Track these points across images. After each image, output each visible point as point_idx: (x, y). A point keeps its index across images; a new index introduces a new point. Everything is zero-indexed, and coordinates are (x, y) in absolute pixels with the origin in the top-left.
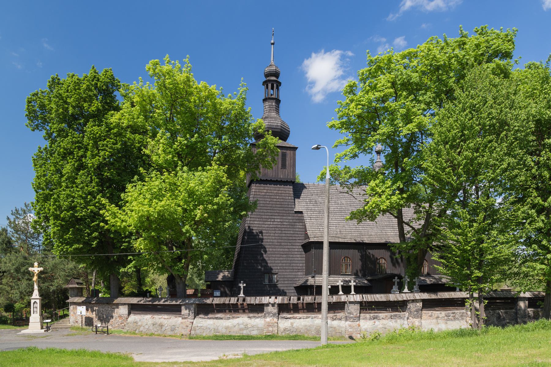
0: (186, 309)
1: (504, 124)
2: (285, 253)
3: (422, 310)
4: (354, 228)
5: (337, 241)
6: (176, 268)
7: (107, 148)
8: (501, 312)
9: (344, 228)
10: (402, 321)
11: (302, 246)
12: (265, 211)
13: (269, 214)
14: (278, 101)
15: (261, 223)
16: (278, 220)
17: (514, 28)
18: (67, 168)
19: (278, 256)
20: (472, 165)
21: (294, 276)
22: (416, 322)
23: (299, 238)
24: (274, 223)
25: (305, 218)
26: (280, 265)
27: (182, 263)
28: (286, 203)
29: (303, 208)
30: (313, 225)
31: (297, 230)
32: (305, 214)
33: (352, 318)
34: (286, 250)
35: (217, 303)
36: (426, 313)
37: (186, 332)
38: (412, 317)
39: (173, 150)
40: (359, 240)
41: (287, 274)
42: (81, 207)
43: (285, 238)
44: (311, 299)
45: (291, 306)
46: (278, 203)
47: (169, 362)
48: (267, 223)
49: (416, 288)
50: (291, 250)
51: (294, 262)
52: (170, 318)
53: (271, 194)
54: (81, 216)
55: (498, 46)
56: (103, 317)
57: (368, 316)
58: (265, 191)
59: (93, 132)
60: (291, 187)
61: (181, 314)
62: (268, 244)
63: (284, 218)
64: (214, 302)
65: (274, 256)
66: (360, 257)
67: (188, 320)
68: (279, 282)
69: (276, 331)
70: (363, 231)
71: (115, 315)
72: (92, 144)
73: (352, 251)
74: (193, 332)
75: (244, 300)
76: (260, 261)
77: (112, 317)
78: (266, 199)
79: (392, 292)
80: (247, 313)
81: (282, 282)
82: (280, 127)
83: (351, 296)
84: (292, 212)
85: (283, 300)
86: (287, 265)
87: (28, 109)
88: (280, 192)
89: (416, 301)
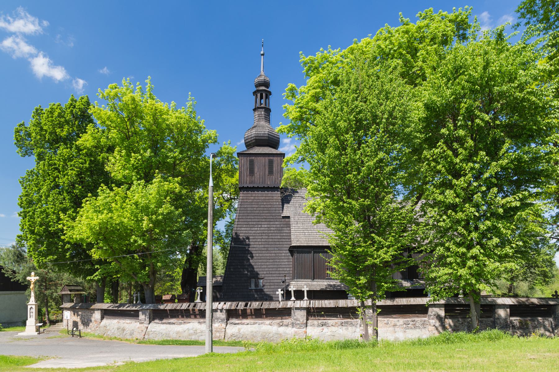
0: (143, 314)
2: (272, 258)
5: (321, 245)
6: (140, 275)
7: (74, 168)
10: (354, 328)
12: (253, 217)
13: (257, 220)
14: (268, 111)
15: (248, 229)
16: (265, 226)
19: (265, 261)
23: (286, 243)
24: (261, 229)
26: (267, 269)
27: (145, 271)
28: (274, 209)
29: (291, 213)
30: (299, 229)
31: (284, 234)
32: (292, 219)
33: (298, 324)
34: (273, 255)
35: (170, 308)
36: (313, 321)
37: (140, 337)
39: (131, 166)
43: (272, 243)
44: (258, 305)
45: (240, 312)
46: (265, 209)
48: (254, 229)
50: (277, 254)
51: (281, 266)
53: (258, 201)
54: (54, 230)
56: (85, 321)
57: (316, 322)
58: (252, 198)
59: (62, 154)
62: (254, 249)
63: (272, 223)
65: (261, 261)
68: (266, 287)
69: (223, 337)
71: (93, 319)
74: (146, 337)
76: (247, 267)
77: (91, 321)
78: (253, 206)
79: (349, 298)
80: (198, 318)
81: (268, 287)
82: (267, 135)
83: (291, 302)
84: (279, 217)
85: (231, 305)
86: (274, 269)
87: (16, 137)
88: (267, 198)
89: (369, 308)
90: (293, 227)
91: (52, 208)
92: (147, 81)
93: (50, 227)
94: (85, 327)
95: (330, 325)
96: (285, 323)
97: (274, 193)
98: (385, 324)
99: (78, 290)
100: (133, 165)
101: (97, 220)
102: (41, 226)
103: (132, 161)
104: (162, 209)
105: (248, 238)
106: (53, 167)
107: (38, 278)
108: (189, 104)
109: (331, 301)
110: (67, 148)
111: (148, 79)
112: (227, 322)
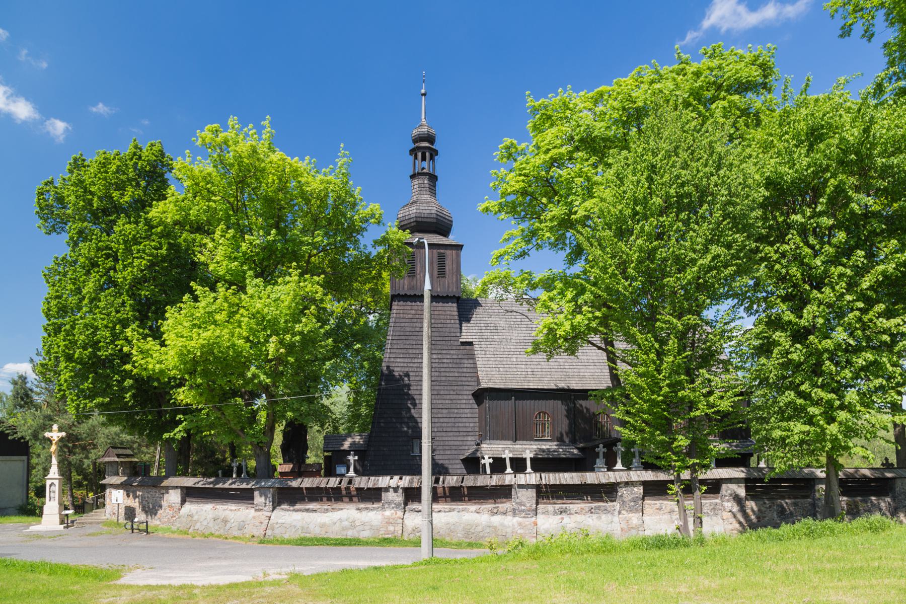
0: (261, 496)
1: (704, 194)
3: (643, 499)
4: (556, 367)
5: (526, 387)
7: (144, 255)
8: (787, 503)
9: (540, 367)
10: (610, 516)
11: (473, 395)
12: (414, 342)
14: (433, 178)
15: (406, 360)
17: (769, 45)
18: (89, 288)
20: (652, 262)
21: (461, 443)
22: (635, 518)
25: (476, 352)
28: (447, 330)
31: (465, 370)
33: (523, 511)
34: (447, 402)
35: (308, 486)
36: (651, 504)
37: (259, 532)
38: (627, 511)
39: (241, 254)
40: (562, 385)
41: (450, 439)
42: (107, 343)
44: (457, 481)
47: (170, 585)
49: (635, 462)
50: (454, 401)
51: (460, 420)
52: (239, 510)
54: (106, 355)
55: (737, 73)
56: (149, 507)
57: (550, 508)
58: (413, 312)
59: (123, 232)
60: (455, 305)
61: (253, 504)
63: (444, 352)
64: (304, 485)
66: (565, 413)
67: (264, 513)
69: (400, 532)
70: (570, 370)
71: (164, 504)
72: (123, 249)
73: (551, 402)
74: (269, 532)
75: (350, 482)
76: (406, 420)
77: (161, 507)
78: (415, 325)
79: (596, 469)
80: (355, 502)
81: (442, 452)
82: (435, 216)
84: (456, 343)
85: (411, 481)
86: (449, 425)
87: (38, 202)
90: (480, 359)
91: (103, 319)
92: (266, 123)
93: (99, 350)
94: (149, 517)
95: (573, 512)
96: (501, 510)
97: (447, 305)
98: (657, 509)
99: (128, 456)
100: (245, 254)
101: (198, 340)
102: (85, 348)
103: (244, 247)
104: (301, 325)
105: (407, 375)
106: (103, 253)
107: (64, 434)
108: (341, 162)
109: (574, 474)
110: (130, 223)
111: (265, 120)
112: (404, 508)
